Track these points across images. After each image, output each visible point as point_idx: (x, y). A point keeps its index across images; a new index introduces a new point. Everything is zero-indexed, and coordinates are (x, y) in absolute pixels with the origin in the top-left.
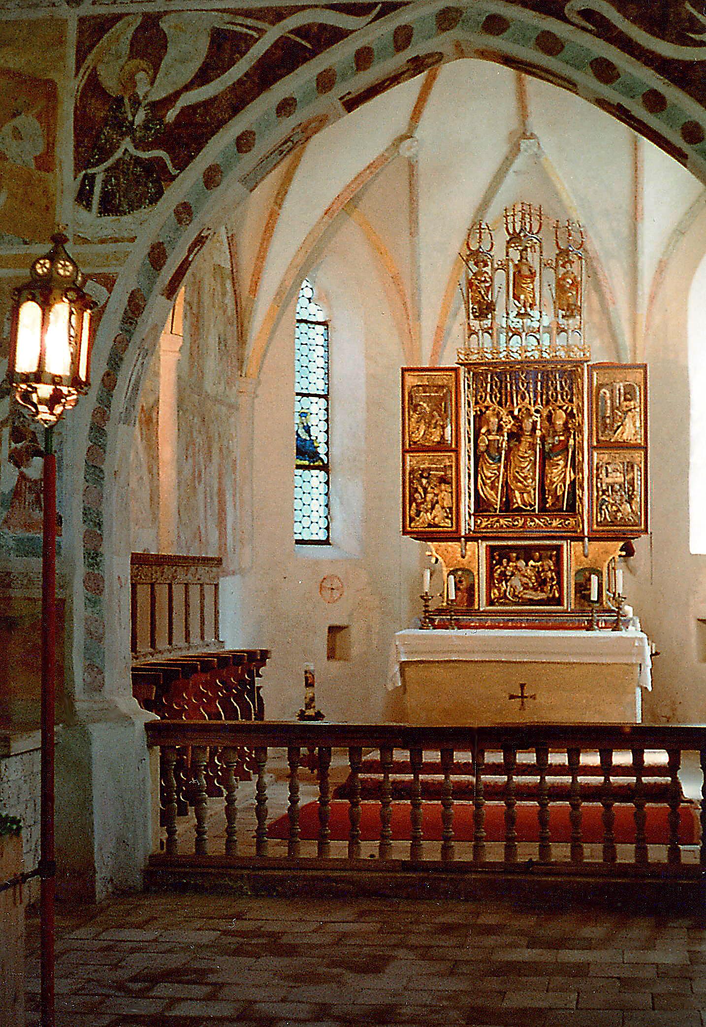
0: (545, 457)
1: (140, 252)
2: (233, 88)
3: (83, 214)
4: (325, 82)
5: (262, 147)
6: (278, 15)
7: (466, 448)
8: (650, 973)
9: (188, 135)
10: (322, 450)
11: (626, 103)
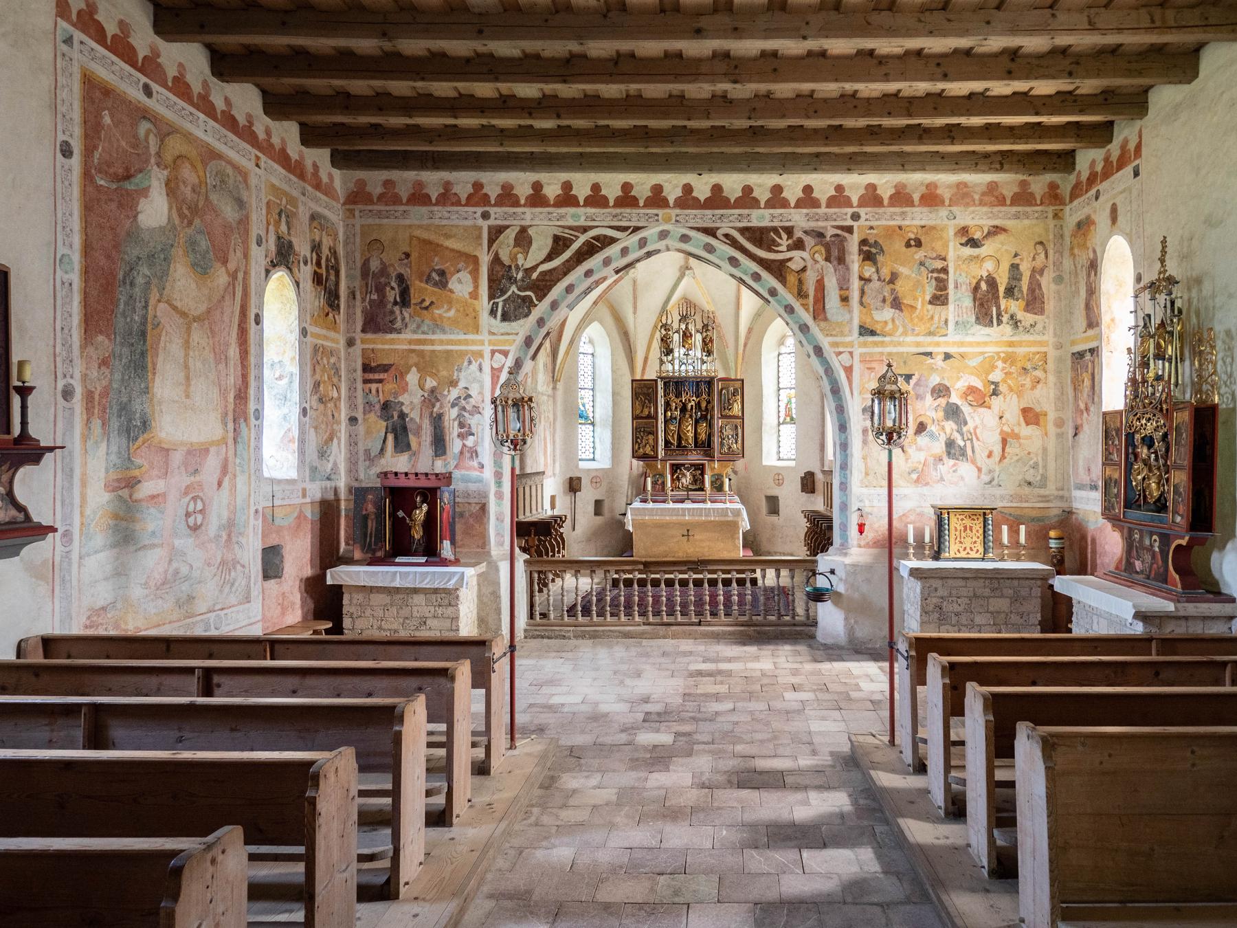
0: (697, 422)
1: (520, 339)
2: (564, 264)
3: (493, 321)
4: (607, 262)
5: (577, 291)
6: (585, 230)
7: (661, 418)
8: (759, 674)
9: (543, 286)
10: (591, 415)
11: (744, 277)
